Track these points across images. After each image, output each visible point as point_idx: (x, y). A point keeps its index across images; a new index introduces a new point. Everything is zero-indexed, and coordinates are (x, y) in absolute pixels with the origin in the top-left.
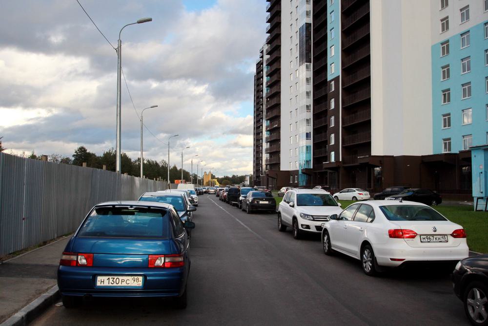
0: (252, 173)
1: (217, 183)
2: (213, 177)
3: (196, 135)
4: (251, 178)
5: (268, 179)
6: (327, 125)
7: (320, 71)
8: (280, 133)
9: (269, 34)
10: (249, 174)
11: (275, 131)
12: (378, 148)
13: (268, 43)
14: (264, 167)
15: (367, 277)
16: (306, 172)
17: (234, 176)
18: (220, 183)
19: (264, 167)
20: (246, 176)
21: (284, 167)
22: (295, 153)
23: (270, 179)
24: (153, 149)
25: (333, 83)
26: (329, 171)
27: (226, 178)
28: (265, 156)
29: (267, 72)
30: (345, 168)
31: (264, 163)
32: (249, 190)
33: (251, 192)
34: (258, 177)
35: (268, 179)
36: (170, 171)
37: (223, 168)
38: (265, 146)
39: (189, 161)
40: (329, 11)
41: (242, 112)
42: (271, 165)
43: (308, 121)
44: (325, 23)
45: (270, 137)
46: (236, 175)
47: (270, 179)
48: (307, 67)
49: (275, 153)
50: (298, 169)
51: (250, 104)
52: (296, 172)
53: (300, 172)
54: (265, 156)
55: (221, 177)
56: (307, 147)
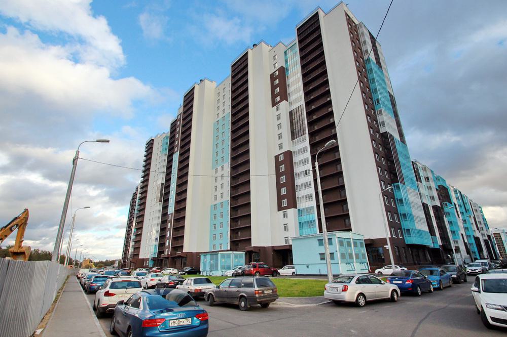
0: (121, 258)
1: (93, 266)
2: (91, 261)
3: (84, 228)
4: (119, 262)
5: (131, 264)
6: (164, 243)
7: (165, 208)
8: (141, 237)
9: (142, 184)
10: (118, 259)
11: (140, 229)
12: (186, 249)
13: (141, 183)
14: (129, 256)
15: (365, 307)
16: (154, 259)
17: (107, 260)
18: (96, 266)
19: (129, 256)
20: (116, 260)
21: (141, 257)
22: (148, 250)
23: (132, 263)
24: (43, 238)
25: (170, 215)
26: (164, 259)
27: (101, 262)
28: (131, 250)
29: (137, 209)
30: (172, 257)
31: (130, 253)
32: (119, 272)
33: (120, 272)
34: (124, 261)
35: (131, 264)
36: (61, 256)
37: (102, 254)
38: (133, 237)
39: (75, 250)
40: (173, 168)
41: (120, 214)
42: (134, 248)
43: (159, 217)
44: (172, 160)
45: (136, 239)
46: (108, 260)
47: (132, 263)
48: (160, 204)
49: (137, 249)
50: (149, 257)
51: (127, 208)
52: (148, 259)
53: (150, 259)
54: (131, 250)
55: (97, 261)
56: (155, 245)
